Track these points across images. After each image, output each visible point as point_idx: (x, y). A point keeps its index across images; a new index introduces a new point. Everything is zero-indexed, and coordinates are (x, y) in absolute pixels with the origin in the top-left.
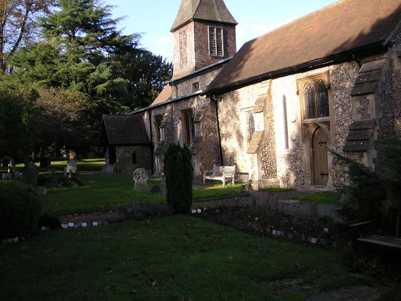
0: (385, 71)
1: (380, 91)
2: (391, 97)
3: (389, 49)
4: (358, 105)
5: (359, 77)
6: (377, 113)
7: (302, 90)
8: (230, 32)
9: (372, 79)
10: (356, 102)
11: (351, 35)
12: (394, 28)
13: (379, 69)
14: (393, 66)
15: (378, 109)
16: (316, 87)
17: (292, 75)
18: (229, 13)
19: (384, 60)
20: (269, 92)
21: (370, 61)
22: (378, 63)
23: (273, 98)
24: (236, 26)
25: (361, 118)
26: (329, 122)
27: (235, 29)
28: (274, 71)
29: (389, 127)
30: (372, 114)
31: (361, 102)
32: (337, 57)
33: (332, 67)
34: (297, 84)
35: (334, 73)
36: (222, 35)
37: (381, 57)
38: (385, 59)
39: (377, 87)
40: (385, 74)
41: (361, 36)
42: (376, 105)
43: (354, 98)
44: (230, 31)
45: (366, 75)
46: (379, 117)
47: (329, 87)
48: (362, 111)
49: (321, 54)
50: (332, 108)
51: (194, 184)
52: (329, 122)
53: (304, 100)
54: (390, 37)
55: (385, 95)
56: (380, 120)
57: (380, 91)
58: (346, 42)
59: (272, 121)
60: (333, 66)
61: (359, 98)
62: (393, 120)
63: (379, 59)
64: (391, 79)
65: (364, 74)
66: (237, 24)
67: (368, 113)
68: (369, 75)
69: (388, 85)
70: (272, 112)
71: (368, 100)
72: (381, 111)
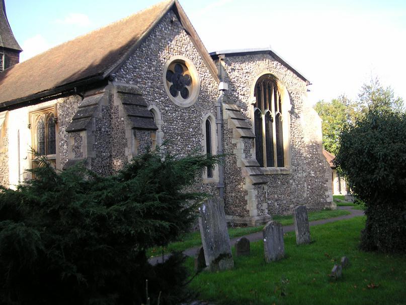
0: (103, 106)
1: (94, 128)
2: (109, 135)
3: (110, 83)
4: (72, 142)
5: (79, 112)
6: (89, 151)
7: (35, 124)
8: (13, 59)
9: (87, 115)
10: (71, 140)
11: (82, 66)
12: (117, 61)
13: (96, 104)
14: (113, 102)
15: (91, 147)
16: (47, 121)
17: (26, 107)
18: (13, 38)
19: (102, 95)
20: (4, 124)
21: (91, 95)
22: (96, 97)
23: (8, 132)
24: (20, 54)
25: (75, 157)
26: (55, 160)
27: (19, 57)
28: (8, 101)
29: (104, 167)
30: (85, 153)
31: (75, 139)
32: (66, 89)
33: (60, 100)
34: (30, 117)
35: (62, 106)
36: (3, 62)
37: (101, 91)
38: (103, 94)
39: (90, 123)
40: (103, 110)
41: (91, 68)
42: (89, 143)
43: (70, 134)
44: (13, 58)
45: (84, 110)
46: (91, 156)
47: (56, 122)
48: (76, 149)
49: (49, 85)
50: (58, 144)
51: (310, 221)
52: (55, 160)
53: (36, 135)
54: (109, 71)
55: (101, 133)
56: (93, 159)
57: (94, 128)
58: (74, 75)
59: (6, 156)
60: (60, 99)
61: (74, 134)
62: (111, 160)
63: (99, 93)
64: (110, 115)
65: (83, 108)
66: (21, 51)
67: (81, 151)
68: (86, 111)
69: (105, 121)
70: (6, 147)
71: (81, 137)
72: (95, 149)
